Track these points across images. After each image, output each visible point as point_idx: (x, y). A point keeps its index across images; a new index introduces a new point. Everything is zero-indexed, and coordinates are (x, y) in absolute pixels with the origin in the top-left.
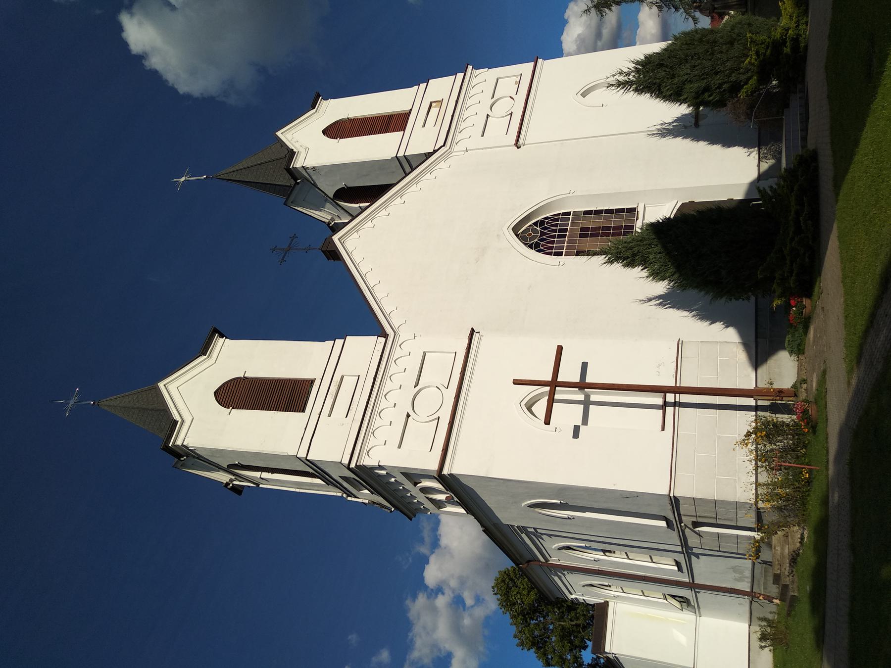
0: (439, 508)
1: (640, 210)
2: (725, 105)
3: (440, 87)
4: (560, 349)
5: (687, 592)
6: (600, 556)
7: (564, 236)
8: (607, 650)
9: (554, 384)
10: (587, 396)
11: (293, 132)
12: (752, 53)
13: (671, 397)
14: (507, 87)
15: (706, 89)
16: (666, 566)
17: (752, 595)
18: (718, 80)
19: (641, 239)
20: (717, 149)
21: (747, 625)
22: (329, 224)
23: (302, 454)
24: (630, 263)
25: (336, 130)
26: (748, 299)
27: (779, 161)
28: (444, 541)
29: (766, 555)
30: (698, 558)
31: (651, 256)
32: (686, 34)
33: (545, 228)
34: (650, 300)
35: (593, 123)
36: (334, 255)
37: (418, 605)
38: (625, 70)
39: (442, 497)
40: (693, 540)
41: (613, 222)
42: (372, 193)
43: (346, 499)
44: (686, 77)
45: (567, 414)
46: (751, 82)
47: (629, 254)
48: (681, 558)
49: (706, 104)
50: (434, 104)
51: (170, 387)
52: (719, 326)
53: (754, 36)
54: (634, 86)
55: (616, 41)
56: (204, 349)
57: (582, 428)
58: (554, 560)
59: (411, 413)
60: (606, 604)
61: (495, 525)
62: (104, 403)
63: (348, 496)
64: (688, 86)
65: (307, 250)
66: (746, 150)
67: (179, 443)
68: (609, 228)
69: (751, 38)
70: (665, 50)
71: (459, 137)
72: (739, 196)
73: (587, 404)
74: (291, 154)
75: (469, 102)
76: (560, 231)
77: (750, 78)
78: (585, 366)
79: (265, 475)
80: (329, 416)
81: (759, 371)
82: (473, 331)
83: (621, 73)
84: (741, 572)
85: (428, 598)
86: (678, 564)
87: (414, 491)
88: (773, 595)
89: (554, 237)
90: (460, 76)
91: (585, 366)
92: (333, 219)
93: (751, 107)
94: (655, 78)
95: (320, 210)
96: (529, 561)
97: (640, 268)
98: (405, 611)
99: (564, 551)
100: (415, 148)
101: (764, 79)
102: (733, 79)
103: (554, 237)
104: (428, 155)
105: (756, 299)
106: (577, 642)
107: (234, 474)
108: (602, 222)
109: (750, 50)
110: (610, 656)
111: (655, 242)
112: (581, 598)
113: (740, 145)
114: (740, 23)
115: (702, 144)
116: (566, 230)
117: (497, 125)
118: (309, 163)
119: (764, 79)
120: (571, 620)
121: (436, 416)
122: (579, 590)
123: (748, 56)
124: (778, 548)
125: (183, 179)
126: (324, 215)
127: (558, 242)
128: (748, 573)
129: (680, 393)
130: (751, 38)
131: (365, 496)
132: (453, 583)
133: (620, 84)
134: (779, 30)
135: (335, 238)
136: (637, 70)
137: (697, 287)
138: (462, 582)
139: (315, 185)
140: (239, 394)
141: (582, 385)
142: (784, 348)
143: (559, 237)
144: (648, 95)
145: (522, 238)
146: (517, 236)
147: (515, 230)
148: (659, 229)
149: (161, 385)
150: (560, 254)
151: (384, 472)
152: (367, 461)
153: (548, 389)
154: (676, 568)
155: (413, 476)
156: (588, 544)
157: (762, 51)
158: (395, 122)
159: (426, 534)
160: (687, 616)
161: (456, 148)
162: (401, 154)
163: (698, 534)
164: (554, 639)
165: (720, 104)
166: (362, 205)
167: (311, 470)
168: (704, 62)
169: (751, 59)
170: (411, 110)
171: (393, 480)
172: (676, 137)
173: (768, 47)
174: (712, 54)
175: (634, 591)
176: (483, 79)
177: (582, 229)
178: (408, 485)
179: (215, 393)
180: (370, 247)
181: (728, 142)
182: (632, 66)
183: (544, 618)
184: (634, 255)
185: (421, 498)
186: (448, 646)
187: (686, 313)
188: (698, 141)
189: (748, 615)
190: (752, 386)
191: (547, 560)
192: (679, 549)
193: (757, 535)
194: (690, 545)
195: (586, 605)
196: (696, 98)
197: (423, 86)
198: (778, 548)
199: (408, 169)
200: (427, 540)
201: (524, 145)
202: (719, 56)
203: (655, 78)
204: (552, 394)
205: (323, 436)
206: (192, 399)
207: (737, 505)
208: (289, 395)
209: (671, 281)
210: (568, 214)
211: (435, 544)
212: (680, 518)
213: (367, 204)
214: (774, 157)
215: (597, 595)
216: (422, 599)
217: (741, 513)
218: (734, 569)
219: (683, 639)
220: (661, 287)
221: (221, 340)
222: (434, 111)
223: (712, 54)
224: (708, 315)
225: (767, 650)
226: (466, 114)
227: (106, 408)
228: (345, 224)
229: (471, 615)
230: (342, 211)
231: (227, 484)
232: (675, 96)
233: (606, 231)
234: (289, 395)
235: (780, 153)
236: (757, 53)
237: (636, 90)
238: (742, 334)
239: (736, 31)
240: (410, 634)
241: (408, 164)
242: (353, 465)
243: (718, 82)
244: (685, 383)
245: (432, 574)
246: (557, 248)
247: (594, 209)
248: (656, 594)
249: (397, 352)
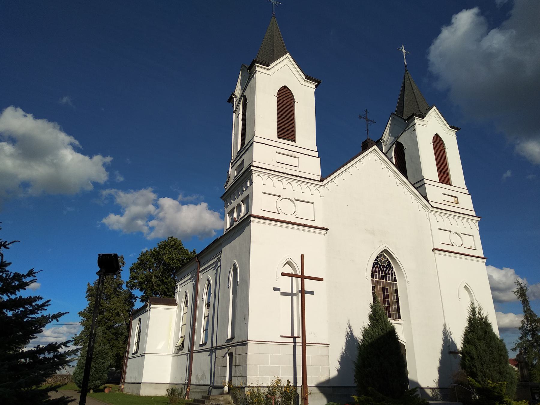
0: (228, 214)
1: (400, 322)
2: (462, 369)
3: (466, 202)
4: (321, 280)
5: (186, 349)
6: (205, 301)
7: (383, 279)
8: (152, 306)
9: (303, 277)
10: (296, 295)
11: (436, 116)
12: (495, 385)
13: (299, 341)
14: (468, 242)
15: (472, 358)
16: (200, 338)
17: (188, 385)
18: (478, 365)
19: (386, 323)
20: (438, 364)
21: (169, 382)
22: (381, 139)
23: (256, 139)
24: (372, 318)
25: (438, 142)
26: (356, 382)
27: (432, 399)
28: (185, 207)
29: (214, 392)
30: (209, 355)
31: (376, 330)
32: (504, 346)
33: (387, 268)
34: (350, 328)
35: (451, 293)
36: (365, 147)
37: (149, 194)
38: (482, 312)
39: (235, 215)
40: (220, 353)
41: (392, 306)
42: (401, 165)
43: (230, 162)
44: (479, 347)
45: (285, 284)
46: (477, 383)
47: (377, 317)
48: (208, 346)
49: (463, 358)
50: (456, 199)
51: (287, 60)
52: (338, 366)
53: (504, 385)
54: (472, 317)
55: (500, 305)
56: (309, 77)
57: (279, 293)
58: (201, 276)
59: (281, 198)
60: (175, 304)
61: (221, 244)
62: (274, 21)
63: (232, 163)
64: (474, 348)
65: (367, 130)
66: (437, 381)
67: (257, 69)
68: (388, 304)
69: (504, 384)
70: (495, 335)
71: (437, 215)
72: (410, 376)
73: (292, 295)
74: (423, 116)
75: (458, 220)
76: (386, 276)
77: (479, 383)
78: (312, 293)
79: (241, 116)
80: (277, 152)
81: (315, 388)
82: (327, 230)
83: (480, 309)
84: (202, 379)
85: (154, 200)
86: (204, 344)
87: (238, 200)
88: (190, 396)
89: (382, 273)
90: (474, 214)
91: (312, 293)
92: (384, 141)
93: (462, 384)
94: (477, 329)
95: (389, 134)
96: (199, 262)
97: (369, 324)
98: (145, 187)
99: (207, 282)
100: (430, 190)
101: (479, 391)
102: (479, 373)
103: (382, 273)
104: (426, 198)
105: (354, 387)
106: (144, 286)
107: (240, 99)
108: (392, 300)
109: (497, 383)
110: (148, 308)
111: (385, 331)
112: (178, 290)
113: (439, 377)
114: (512, 377)
115: (439, 355)
116: (386, 280)
117: (445, 237)
118: (417, 127)
119: (479, 391)
120: (155, 282)
121: (280, 212)
122: (183, 289)
123: (493, 381)
124: (222, 399)
125: (404, 51)
126: (386, 136)
127: (379, 275)
128: (201, 382)
129: (302, 345)
130: (504, 384)
131: (233, 173)
132: (161, 215)
133: (473, 310)
134: (509, 400)
135: (375, 147)
136: (482, 319)
137: (360, 354)
138: (162, 219)
139: (404, 131)
140: (285, 99)
141: (303, 292)
142: (328, 402)
143: (382, 276)
144: (467, 325)
145: (380, 255)
146: (382, 252)
147: (385, 251)
148: (392, 334)
149: (288, 55)
150: (372, 277)
151: (249, 184)
152: (255, 176)
153: (299, 273)
154: (201, 343)
155: (247, 200)
156: (212, 295)
157: (496, 390)
158: (444, 176)
159: (189, 198)
160: (172, 349)
161: (431, 214)
162: (426, 181)
163: (225, 356)
164: (145, 273)
165: (463, 366)
166: (394, 158)
167: (246, 143)
168: (488, 357)
169: (491, 384)
170: (452, 185)
171: (244, 189)
172: (443, 340)
173: (498, 393)
174: (493, 362)
175: (187, 319)
176: (473, 227)
177: (387, 289)
178: (242, 197)
179: (285, 86)
180: (372, 167)
181: (441, 370)
182: (484, 316)
183: (156, 267)
184: (377, 320)
185: (234, 204)
186: (127, 213)
187: (344, 349)
188: (441, 353)
189: (173, 382)
190: (308, 385)
191: (201, 272)
192: (214, 345)
193: (226, 388)
194: (217, 351)
195: (174, 293)
196: (467, 353)
197: (467, 192)
198: (222, 399)
199: (417, 186)
200: (185, 199)
201: (434, 253)
202: (492, 365)
203: (477, 329)
204: (297, 276)
205: (266, 151)
206: (282, 73)
207: (245, 377)
208: (286, 129)
209: (362, 340)
210: (396, 281)
211: (183, 203)
212: (235, 346)
213: (394, 163)
214: (433, 396)
215: (180, 299)
216: (153, 196)
217: (240, 379)
218: (204, 375)
219: (160, 347)
220: (358, 335)
221: (314, 86)
222: (452, 199)
223: (493, 362)
224: (344, 360)
225: (167, 393)
226: (451, 219)
227: (271, 21)
228: (381, 149)
229: (144, 225)
230: (389, 147)
231: (234, 95)
232: (467, 340)
233: (387, 302)
234: (286, 129)
235: (436, 400)
236: (495, 387)
237: (470, 318)
238: (334, 379)
239: (508, 375)
240: (132, 191)
241: (419, 185)
242: (252, 168)
243: (477, 365)
244: (308, 348)
245: (167, 202)
246: (376, 275)
247: (399, 295)
248: (186, 332)
249: (313, 188)
